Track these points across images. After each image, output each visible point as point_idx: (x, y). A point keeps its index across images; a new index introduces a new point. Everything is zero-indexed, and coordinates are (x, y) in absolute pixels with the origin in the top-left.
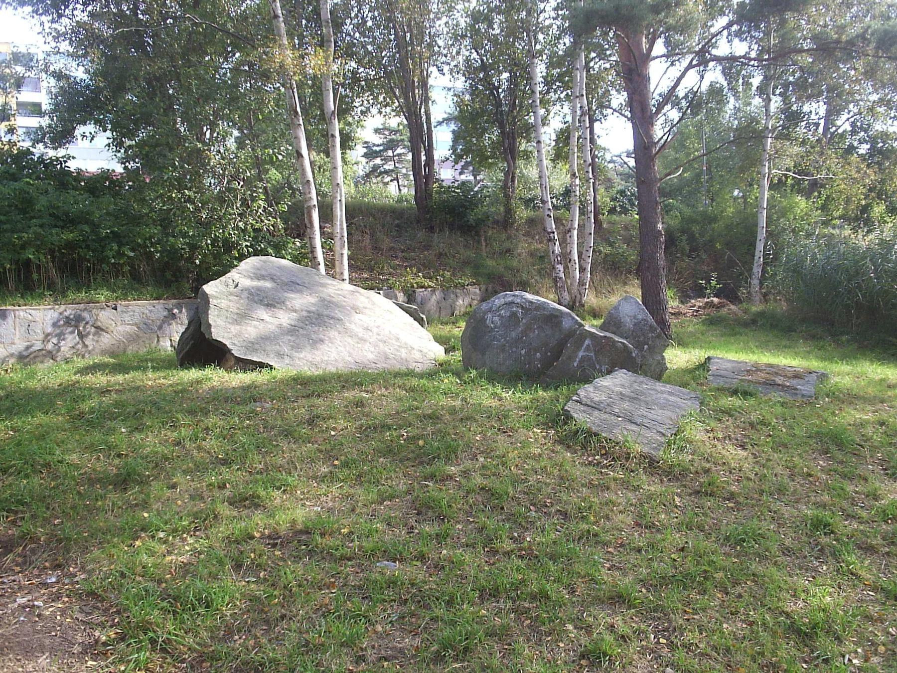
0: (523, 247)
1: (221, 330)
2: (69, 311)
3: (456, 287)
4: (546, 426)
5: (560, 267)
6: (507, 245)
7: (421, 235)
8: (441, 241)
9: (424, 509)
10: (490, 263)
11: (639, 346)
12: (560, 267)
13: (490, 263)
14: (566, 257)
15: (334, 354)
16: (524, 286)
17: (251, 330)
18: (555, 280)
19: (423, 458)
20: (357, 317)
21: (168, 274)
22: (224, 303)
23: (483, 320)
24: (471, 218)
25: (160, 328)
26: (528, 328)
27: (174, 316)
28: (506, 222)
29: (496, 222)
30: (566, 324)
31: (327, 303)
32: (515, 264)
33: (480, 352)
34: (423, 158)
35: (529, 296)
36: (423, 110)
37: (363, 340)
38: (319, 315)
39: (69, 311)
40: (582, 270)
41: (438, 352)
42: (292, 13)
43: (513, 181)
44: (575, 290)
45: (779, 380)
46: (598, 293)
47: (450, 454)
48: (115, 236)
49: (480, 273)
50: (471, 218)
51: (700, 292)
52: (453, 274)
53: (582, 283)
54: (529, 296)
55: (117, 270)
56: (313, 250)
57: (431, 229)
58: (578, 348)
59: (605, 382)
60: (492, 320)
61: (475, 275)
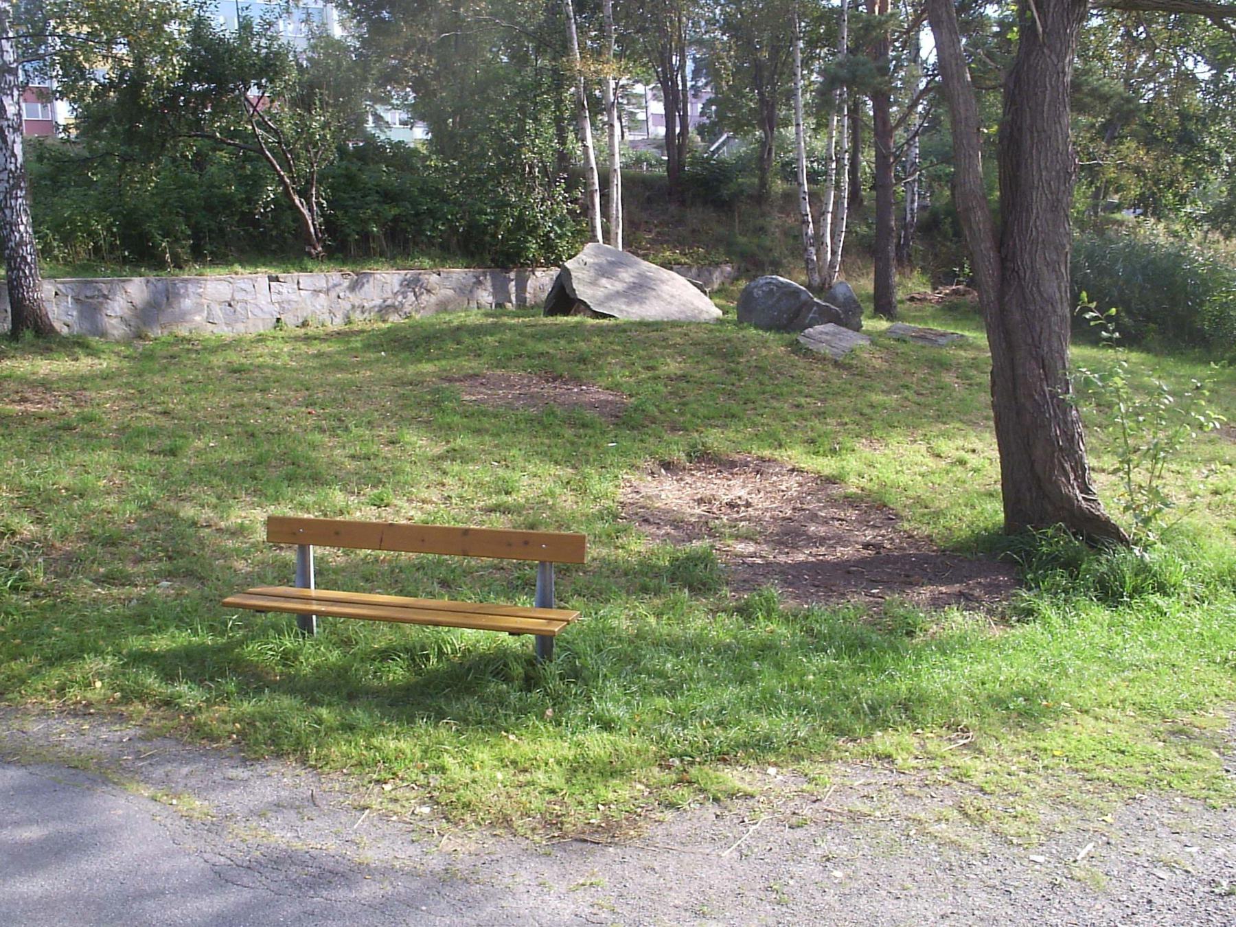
0: (775, 221)
1: (583, 291)
2: (410, 274)
3: (710, 265)
4: (787, 346)
5: (812, 250)
6: (760, 222)
7: (673, 208)
8: (696, 216)
9: (730, 372)
10: (742, 239)
11: (846, 312)
12: (812, 250)
13: (742, 239)
14: (818, 239)
15: (651, 310)
16: (776, 267)
17: (600, 293)
18: (808, 261)
19: (725, 356)
20: (665, 287)
21: (472, 247)
22: (580, 276)
23: (751, 293)
24: (725, 193)
25: (471, 291)
26: (779, 300)
27: (479, 283)
28: (760, 197)
29: (750, 197)
30: (803, 297)
31: (641, 275)
32: (768, 243)
33: (748, 310)
34: (678, 130)
35: (781, 279)
36: (679, 78)
37: (670, 303)
38: (641, 286)
39: (410, 274)
40: (834, 253)
41: (718, 313)
42: (580, 5)
43: (769, 154)
44: (825, 272)
45: (929, 336)
46: (849, 276)
47: (740, 355)
48: (430, 212)
49: (732, 250)
50: (725, 193)
51: (950, 278)
52: (708, 252)
53: (832, 266)
54: (781, 279)
55: (430, 242)
56: (593, 229)
57: (683, 203)
58: (809, 312)
59: (819, 328)
60: (757, 293)
61: (728, 253)
